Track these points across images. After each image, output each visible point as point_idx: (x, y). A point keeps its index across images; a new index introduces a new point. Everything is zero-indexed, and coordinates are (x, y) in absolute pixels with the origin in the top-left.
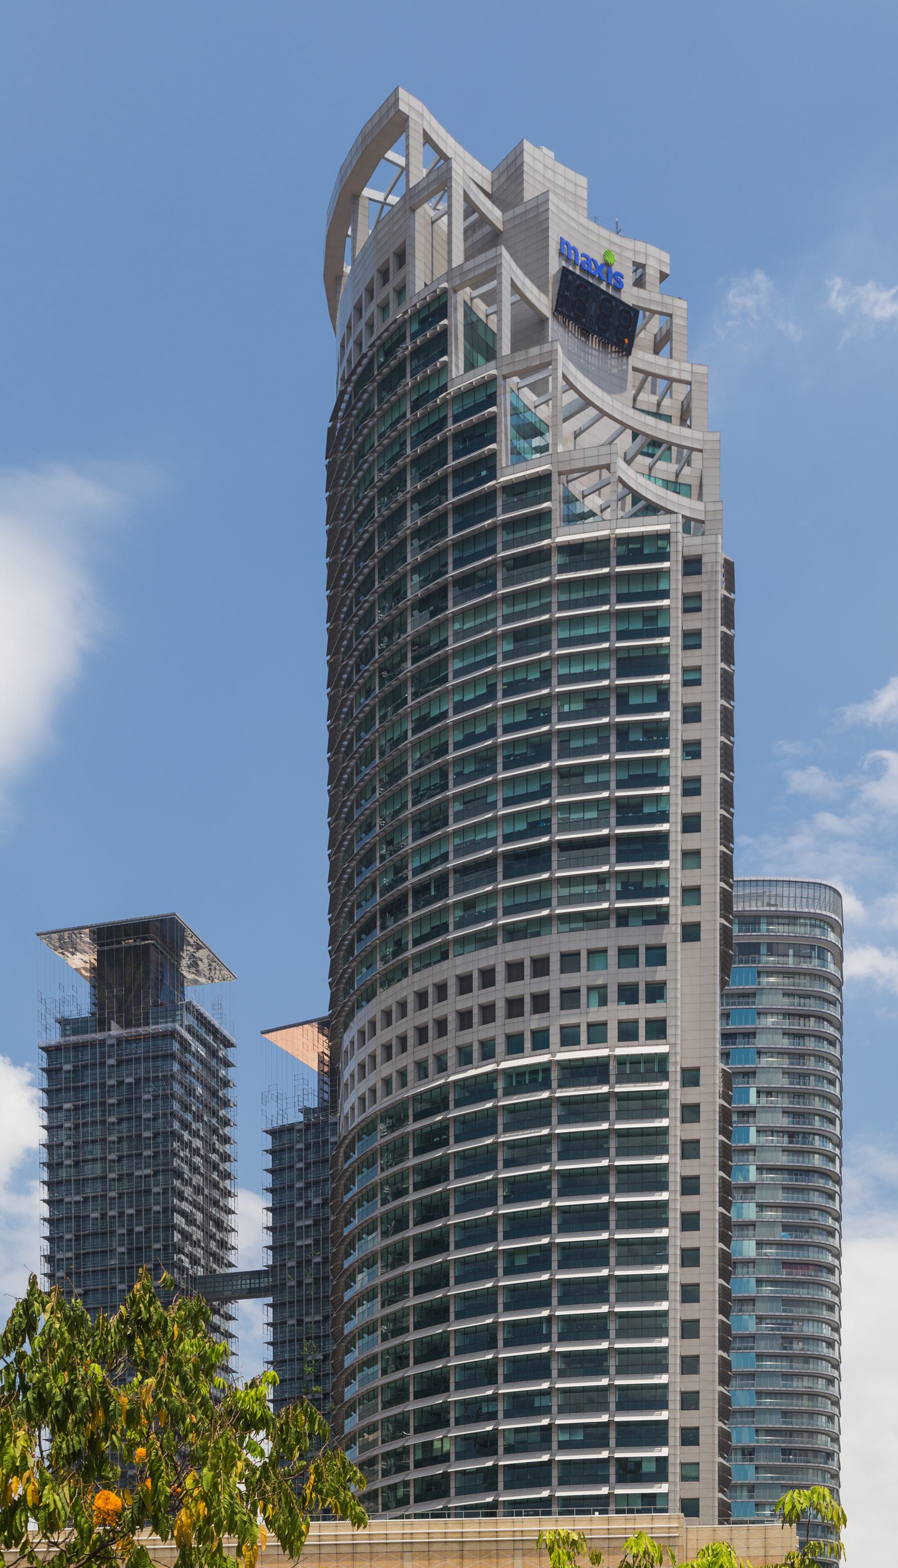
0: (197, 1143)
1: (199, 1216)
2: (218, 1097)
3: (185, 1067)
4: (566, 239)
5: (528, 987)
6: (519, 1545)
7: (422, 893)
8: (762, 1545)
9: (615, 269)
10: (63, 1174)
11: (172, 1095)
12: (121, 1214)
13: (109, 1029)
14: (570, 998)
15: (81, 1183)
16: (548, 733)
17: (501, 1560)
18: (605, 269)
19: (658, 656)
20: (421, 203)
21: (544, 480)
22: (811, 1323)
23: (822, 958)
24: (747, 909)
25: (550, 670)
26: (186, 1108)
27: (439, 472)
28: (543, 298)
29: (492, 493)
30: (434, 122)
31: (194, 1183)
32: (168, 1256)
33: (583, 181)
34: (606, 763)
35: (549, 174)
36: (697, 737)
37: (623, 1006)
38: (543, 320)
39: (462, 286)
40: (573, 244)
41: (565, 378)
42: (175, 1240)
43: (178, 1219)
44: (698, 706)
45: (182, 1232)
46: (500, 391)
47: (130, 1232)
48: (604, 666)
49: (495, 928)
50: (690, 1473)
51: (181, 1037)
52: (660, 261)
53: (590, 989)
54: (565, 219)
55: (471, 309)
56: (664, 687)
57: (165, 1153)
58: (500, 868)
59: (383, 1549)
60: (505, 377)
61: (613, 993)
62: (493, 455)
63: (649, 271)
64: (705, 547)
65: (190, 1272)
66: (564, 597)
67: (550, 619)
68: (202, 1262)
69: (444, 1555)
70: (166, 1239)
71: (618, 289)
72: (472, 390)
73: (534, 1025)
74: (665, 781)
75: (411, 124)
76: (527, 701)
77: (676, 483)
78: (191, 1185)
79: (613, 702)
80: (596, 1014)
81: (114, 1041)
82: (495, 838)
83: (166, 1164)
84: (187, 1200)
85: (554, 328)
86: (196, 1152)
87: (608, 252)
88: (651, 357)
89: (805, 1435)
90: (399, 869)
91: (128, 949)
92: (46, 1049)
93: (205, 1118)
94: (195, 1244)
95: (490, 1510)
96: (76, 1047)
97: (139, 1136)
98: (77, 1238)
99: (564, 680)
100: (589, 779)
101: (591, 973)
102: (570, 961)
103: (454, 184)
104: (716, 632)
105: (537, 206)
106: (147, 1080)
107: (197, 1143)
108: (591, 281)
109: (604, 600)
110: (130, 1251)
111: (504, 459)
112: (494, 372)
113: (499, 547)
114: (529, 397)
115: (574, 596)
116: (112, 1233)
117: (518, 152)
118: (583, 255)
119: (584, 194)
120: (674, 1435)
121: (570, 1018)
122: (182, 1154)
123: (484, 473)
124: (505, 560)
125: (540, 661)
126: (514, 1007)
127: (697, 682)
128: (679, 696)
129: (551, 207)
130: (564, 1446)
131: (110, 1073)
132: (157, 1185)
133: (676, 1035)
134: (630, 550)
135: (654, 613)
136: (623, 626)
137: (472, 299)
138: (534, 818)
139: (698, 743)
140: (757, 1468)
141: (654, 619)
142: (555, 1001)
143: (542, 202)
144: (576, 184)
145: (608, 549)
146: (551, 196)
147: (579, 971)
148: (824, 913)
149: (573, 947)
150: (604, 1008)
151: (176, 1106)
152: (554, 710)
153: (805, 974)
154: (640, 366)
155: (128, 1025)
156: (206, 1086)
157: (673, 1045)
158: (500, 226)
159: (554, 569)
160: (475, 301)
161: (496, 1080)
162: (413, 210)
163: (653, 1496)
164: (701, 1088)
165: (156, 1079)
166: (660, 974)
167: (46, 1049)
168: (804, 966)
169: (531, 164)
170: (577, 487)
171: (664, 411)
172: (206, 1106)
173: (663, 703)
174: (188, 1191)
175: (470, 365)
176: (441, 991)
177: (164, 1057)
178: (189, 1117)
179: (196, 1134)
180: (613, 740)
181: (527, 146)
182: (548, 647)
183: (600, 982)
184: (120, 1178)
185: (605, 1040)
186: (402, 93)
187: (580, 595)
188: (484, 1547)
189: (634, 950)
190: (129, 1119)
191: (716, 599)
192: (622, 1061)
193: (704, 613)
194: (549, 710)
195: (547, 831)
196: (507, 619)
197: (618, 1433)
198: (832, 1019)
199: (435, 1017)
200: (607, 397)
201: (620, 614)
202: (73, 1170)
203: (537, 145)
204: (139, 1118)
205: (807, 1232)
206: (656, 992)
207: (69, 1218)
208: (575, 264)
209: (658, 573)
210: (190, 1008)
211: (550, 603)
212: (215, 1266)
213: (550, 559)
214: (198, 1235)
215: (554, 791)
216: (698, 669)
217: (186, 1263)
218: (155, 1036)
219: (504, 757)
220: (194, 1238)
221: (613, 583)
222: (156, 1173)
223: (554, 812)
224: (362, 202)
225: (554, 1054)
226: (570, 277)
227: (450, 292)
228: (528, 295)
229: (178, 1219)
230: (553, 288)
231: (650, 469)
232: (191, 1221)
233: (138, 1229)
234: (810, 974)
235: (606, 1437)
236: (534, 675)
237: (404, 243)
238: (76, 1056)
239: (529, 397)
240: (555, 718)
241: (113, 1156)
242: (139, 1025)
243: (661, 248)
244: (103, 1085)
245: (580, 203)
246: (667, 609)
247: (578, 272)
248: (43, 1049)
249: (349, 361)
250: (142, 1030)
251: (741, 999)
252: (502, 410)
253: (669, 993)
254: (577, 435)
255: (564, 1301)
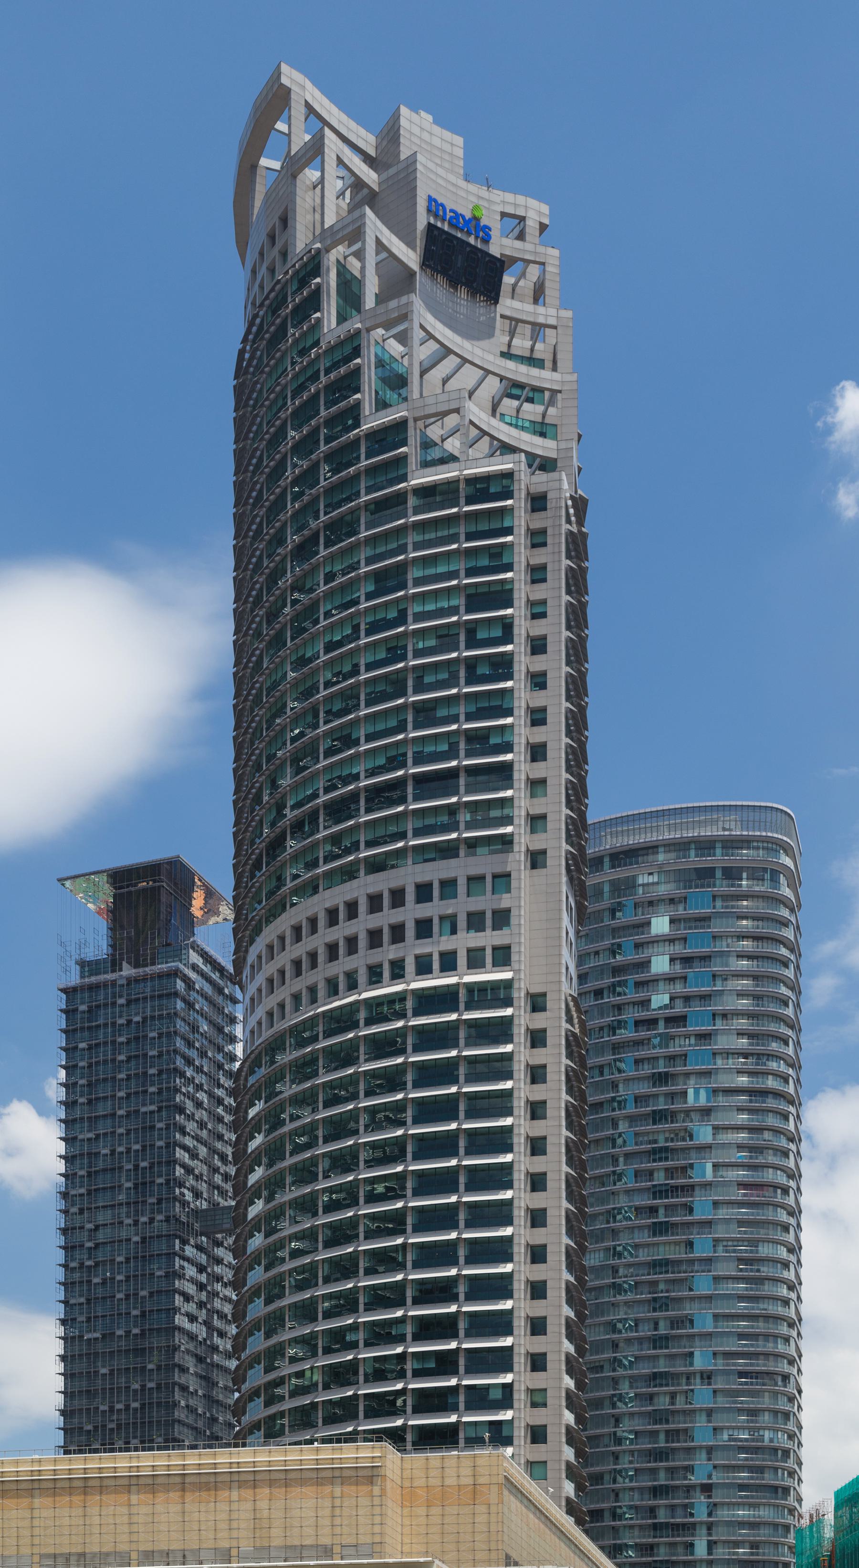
0: (199, 1079)
1: (203, 1151)
2: (223, 1033)
3: (190, 1005)
4: (434, 196)
5: (387, 918)
6: (235, 1477)
7: (298, 827)
8: (471, 1473)
9: (484, 222)
10: (78, 1114)
11: (175, 1032)
12: (129, 1150)
13: (121, 970)
14: (424, 928)
15: (93, 1121)
16: (405, 669)
17: (219, 1493)
18: (474, 222)
19: (503, 591)
20: (301, 169)
21: (401, 426)
22: (766, 1244)
23: (775, 880)
24: (702, 834)
25: (406, 609)
26: (190, 1044)
27: (313, 423)
28: (411, 253)
29: (357, 441)
30: (317, 93)
31: (197, 1118)
32: (171, 1190)
33: (459, 141)
34: (456, 697)
35: (426, 136)
36: (544, 668)
37: (472, 934)
38: (412, 274)
39: (335, 245)
40: (440, 200)
41: (422, 327)
42: (177, 1174)
43: (179, 1153)
44: (544, 638)
45: (184, 1166)
46: (364, 343)
47: (136, 1167)
48: (454, 602)
49: (357, 861)
50: (538, 1398)
51: (185, 975)
52: (540, 213)
53: (442, 918)
54: (433, 177)
55: (344, 267)
56: (508, 621)
57: (168, 1089)
58: (362, 802)
59: (112, 1482)
60: (368, 330)
61: (462, 922)
62: (358, 404)
63: (529, 223)
64: (550, 484)
65: (192, 1206)
66: (419, 538)
67: (405, 559)
68: (205, 1195)
69: (167, 1488)
70: (168, 1175)
71: (486, 240)
72: (341, 344)
73: (392, 956)
74: (509, 712)
75: (293, 96)
76: (386, 639)
77: (542, 423)
78: (193, 1119)
79: (462, 638)
80: (447, 943)
81: (124, 982)
82: (358, 774)
83: (168, 1100)
84: (189, 1134)
85: (420, 279)
86: (199, 1087)
87: (476, 207)
88: (529, 307)
89: (762, 1357)
90: (280, 807)
91: (144, 890)
92: (64, 990)
93: (210, 1054)
94: (198, 1178)
95: (350, 1438)
96: (93, 988)
97: (145, 1073)
98: (89, 1174)
99: (420, 617)
100: (442, 713)
101: (444, 902)
102: (424, 892)
103: (326, 150)
104: (560, 565)
105: (408, 167)
106: (153, 1018)
107: (199, 1079)
108: (459, 235)
109: (454, 538)
110: (136, 1186)
111: (367, 408)
112: (359, 325)
113: (363, 492)
114: (395, 348)
115: (427, 537)
116: (121, 1168)
117: (396, 116)
118: (452, 211)
119: (460, 153)
120: (520, 1361)
121: (424, 947)
122: (184, 1090)
123: (350, 422)
124: (367, 504)
125: (398, 600)
126: (375, 938)
127: (543, 615)
128: (523, 628)
129: (419, 166)
130: (418, 1374)
131: (121, 1012)
132: (160, 1121)
133: (519, 961)
134: (477, 490)
135: (499, 550)
136: (472, 564)
137: (345, 258)
138: (392, 753)
139: (544, 674)
140: (715, 1392)
141: (500, 555)
142: (410, 931)
143: (412, 160)
144: (452, 144)
145: (457, 490)
146: (419, 157)
147: (431, 900)
148: (776, 835)
149: (426, 878)
150: (454, 937)
151: (179, 1043)
152: (410, 648)
153: (758, 897)
154: (508, 313)
155: (136, 966)
156: (210, 1022)
157: (517, 972)
158: (376, 187)
159: (410, 511)
160: (349, 258)
161: (358, 1011)
162: (294, 177)
163: (500, 1423)
164: (548, 1014)
165: (161, 1017)
166: (505, 901)
167: (64, 990)
168: (757, 889)
169: (408, 127)
170: (435, 432)
171: (537, 355)
172: (210, 1041)
173: (507, 637)
174: (191, 1127)
175: (342, 318)
176: (352, 909)
177: (169, 995)
178: (193, 1054)
179: (199, 1070)
180: (462, 674)
181: (404, 111)
182: (404, 586)
183: (450, 911)
184: (128, 1115)
185: (455, 968)
186: (285, 68)
187: (433, 536)
188: (204, 1479)
189: (481, 878)
190: (137, 1057)
191: (560, 534)
192: (471, 988)
193: (549, 548)
194: (405, 647)
195: (403, 765)
196: (369, 561)
197: (468, 1360)
198: (785, 941)
199: (308, 949)
200: (467, 344)
201: (469, 552)
202: (86, 1107)
203: (415, 109)
204: (145, 1055)
205: (762, 1153)
206: (502, 918)
207: (82, 1155)
208: (443, 220)
209: (502, 511)
210: (195, 947)
211: (406, 544)
212: (220, 1200)
213: (406, 502)
214: (200, 1168)
215: (410, 726)
216: (544, 602)
217: (189, 1196)
218: (160, 976)
219: (366, 694)
220: (197, 1172)
221: (462, 522)
222: (160, 1109)
223: (410, 746)
224: (259, 172)
225: (408, 984)
226: (436, 232)
227: (323, 251)
228: (395, 250)
229: (179, 1153)
230: (420, 243)
231: (518, 411)
232: (194, 1156)
233: (144, 1164)
234: (763, 897)
235: (456, 1364)
236: (392, 614)
237: (286, 208)
238: (91, 997)
239: (395, 348)
240: (410, 654)
241: (122, 1094)
242: (146, 966)
243: (540, 200)
244: (114, 1024)
245: (457, 162)
246: (511, 545)
247: (446, 227)
248: (62, 990)
249: (261, 287)
250: (148, 970)
251: (698, 924)
252: (366, 362)
253: (513, 921)
254: (445, 381)
255: (418, 1229)
